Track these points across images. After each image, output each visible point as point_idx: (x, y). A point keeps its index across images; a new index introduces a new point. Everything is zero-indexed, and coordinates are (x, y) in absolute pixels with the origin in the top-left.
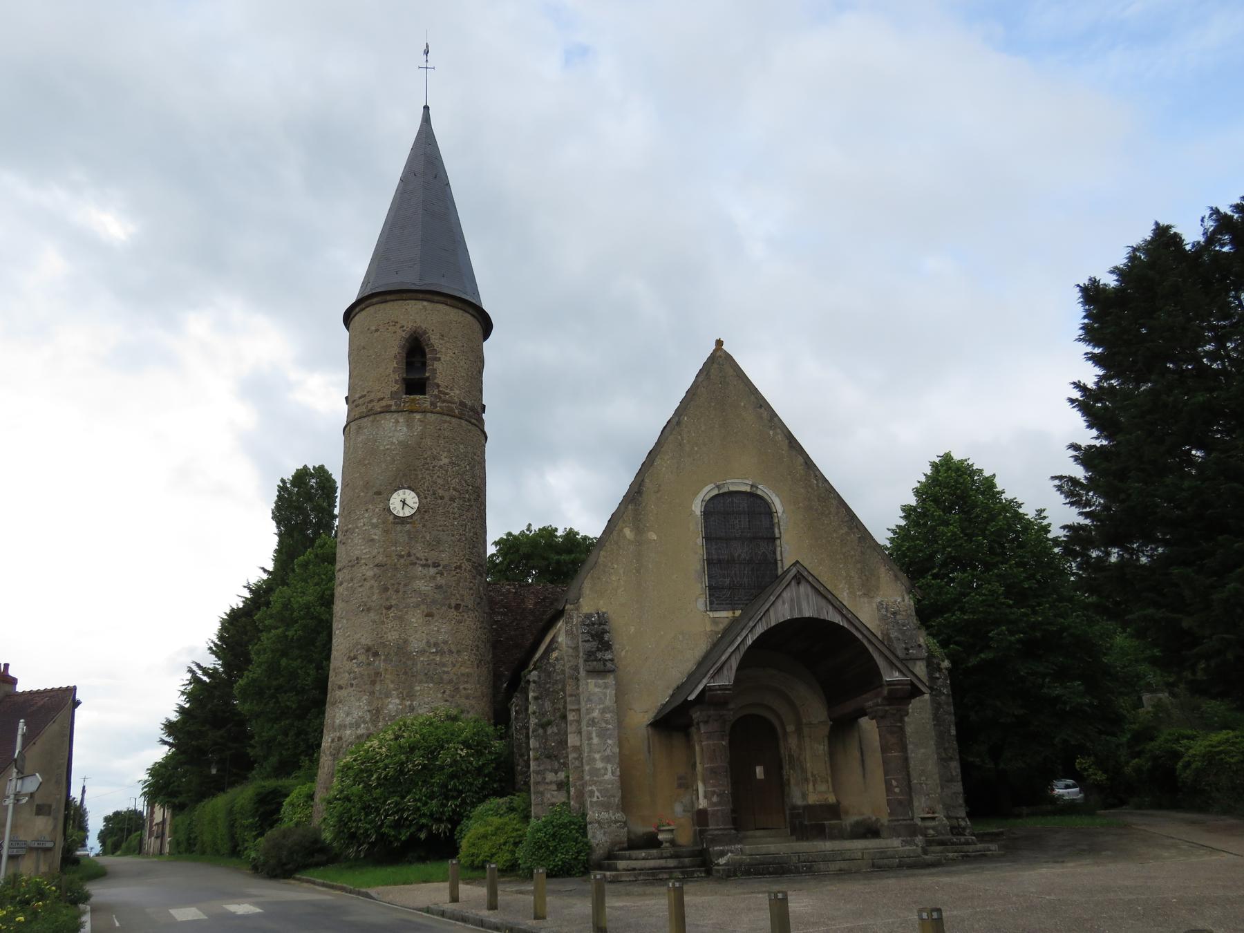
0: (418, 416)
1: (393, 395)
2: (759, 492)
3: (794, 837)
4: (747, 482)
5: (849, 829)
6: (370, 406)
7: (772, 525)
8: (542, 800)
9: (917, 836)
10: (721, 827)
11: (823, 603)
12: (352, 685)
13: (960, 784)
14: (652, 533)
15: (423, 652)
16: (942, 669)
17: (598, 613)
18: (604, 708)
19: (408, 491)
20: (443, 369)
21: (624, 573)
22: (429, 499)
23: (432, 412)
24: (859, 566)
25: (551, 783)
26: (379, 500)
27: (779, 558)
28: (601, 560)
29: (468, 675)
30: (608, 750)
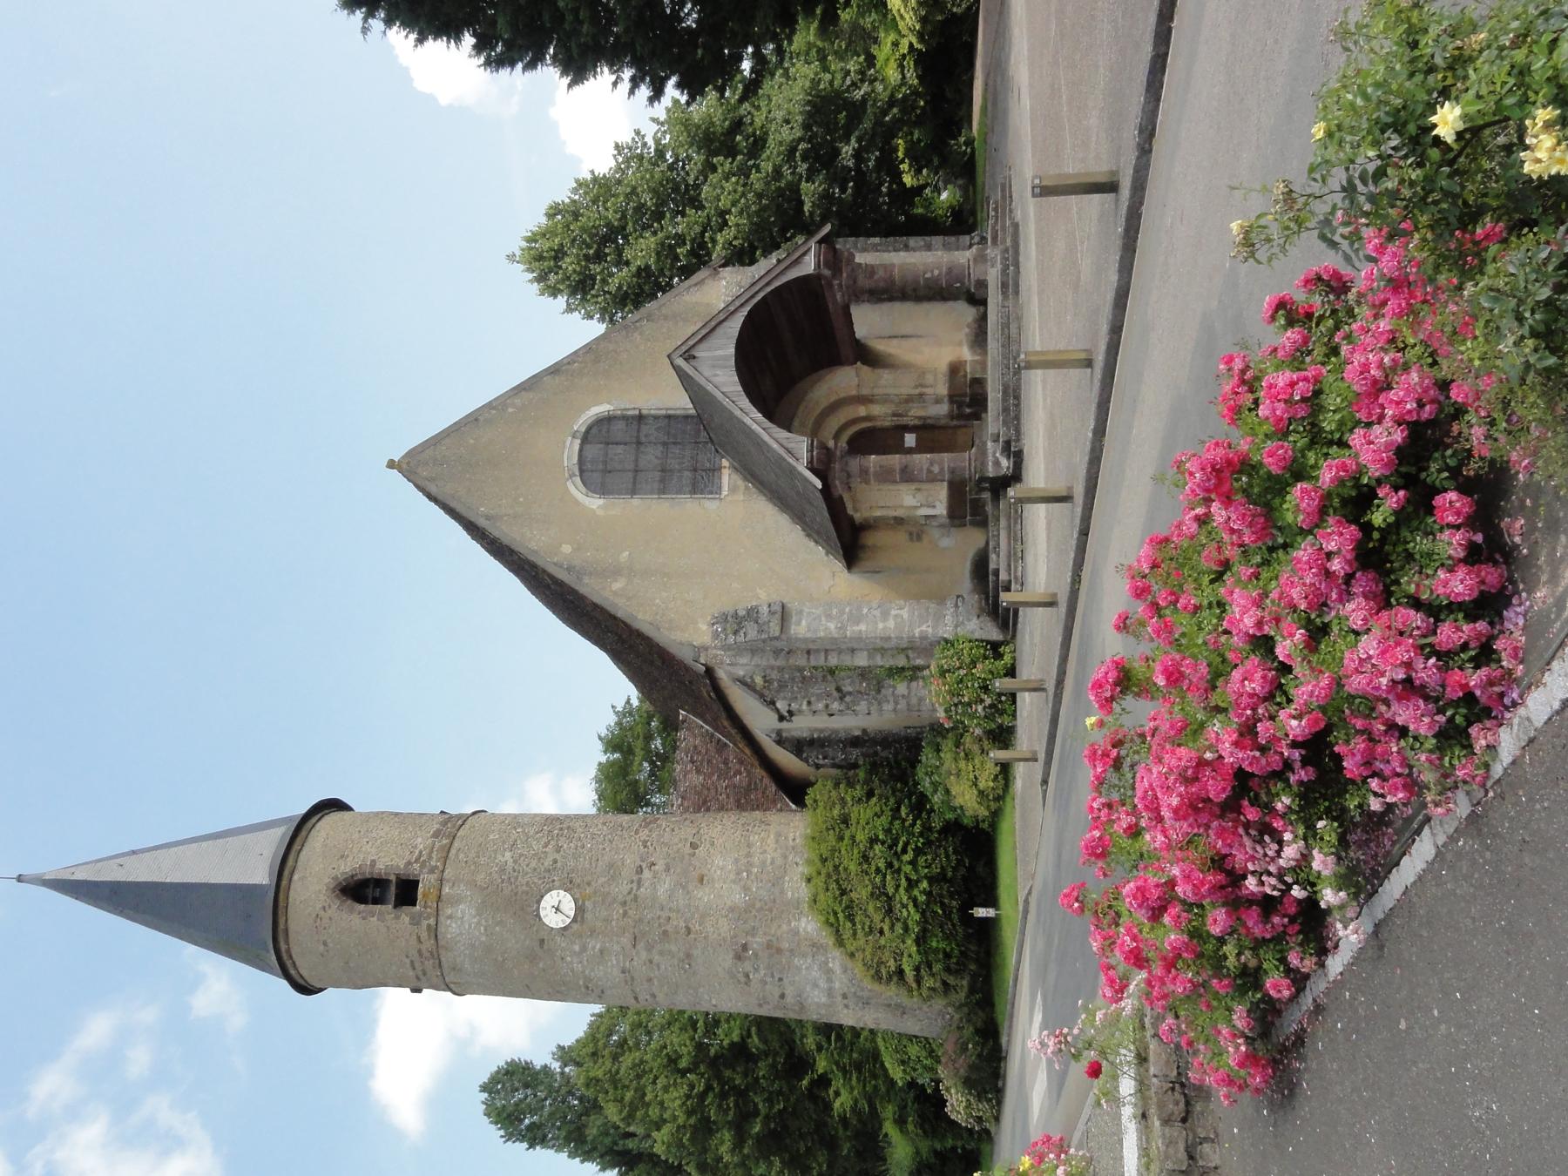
0: (446, 890)
2: (583, 430)
3: (983, 415)
4: (568, 443)
6: (426, 954)
7: (625, 418)
11: (720, 331)
12: (780, 979)
15: (746, 889)
19: (543, 904)
20: (388, 860)
27: (664, 412)
28: (648, 618)
29: (778, 835)
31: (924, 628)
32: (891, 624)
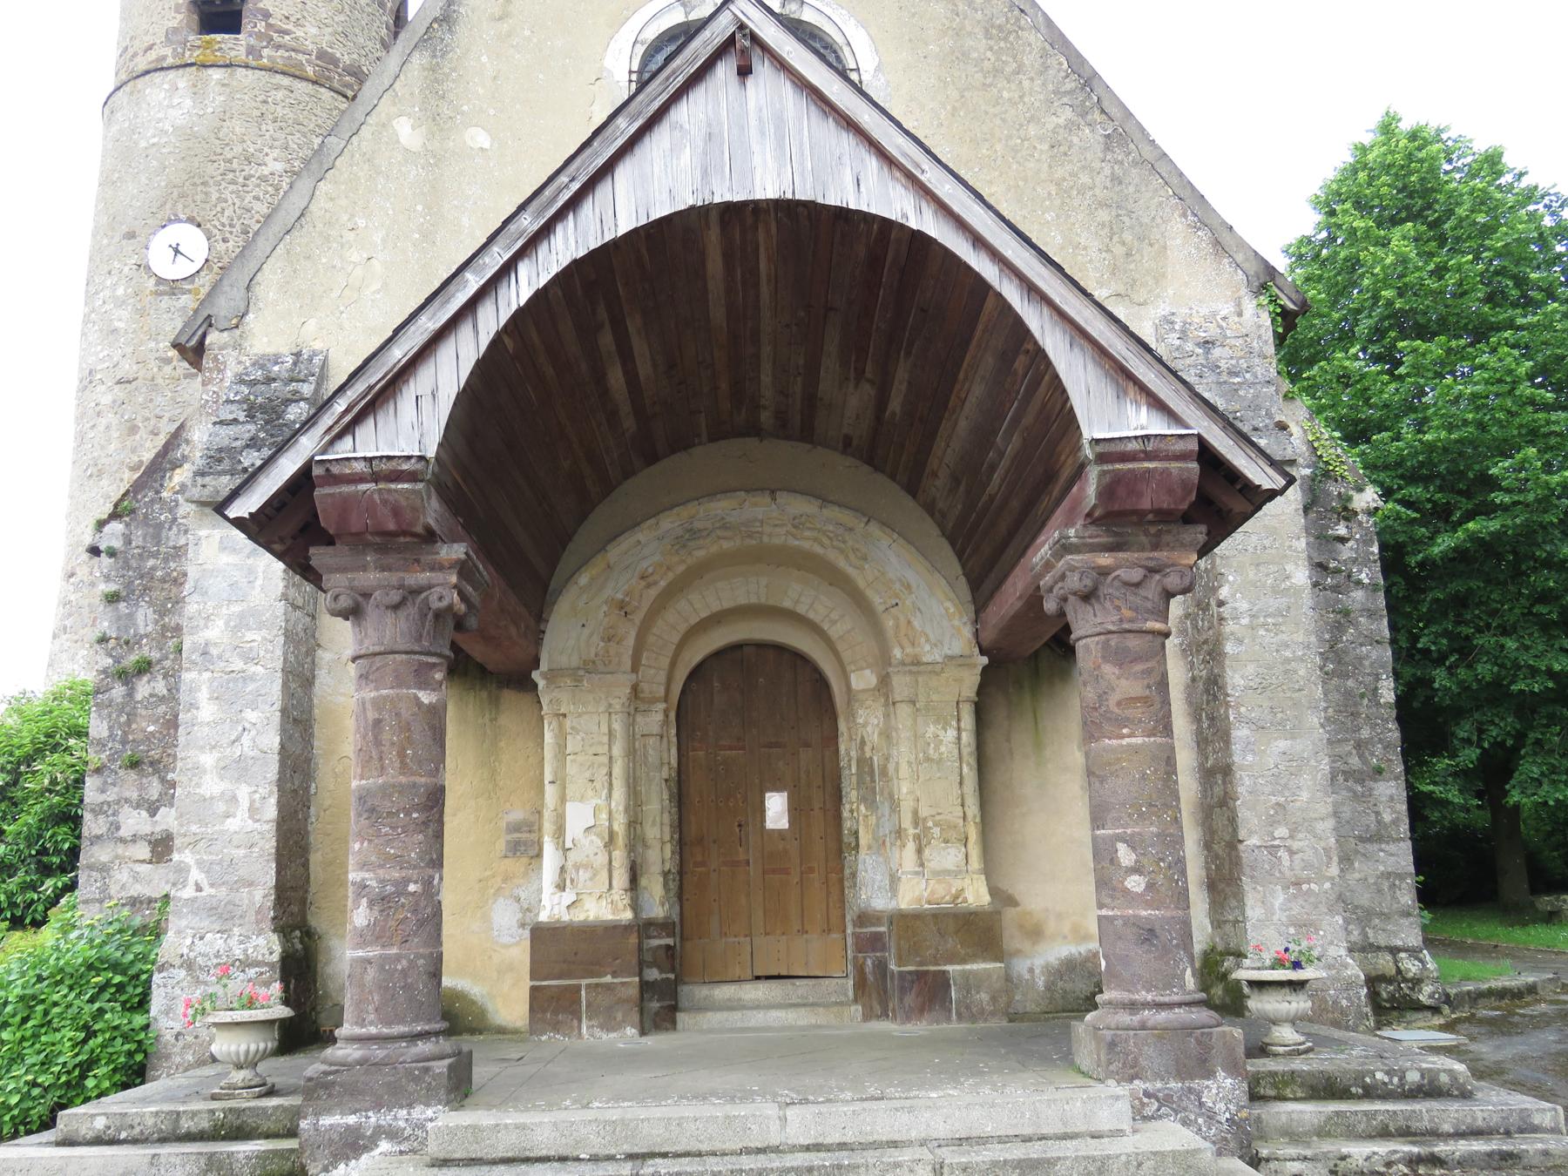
0: (216, 74)
1: (169, 36)
5: (1041, 983)
8: (104, 889)
9: (1210, 1074)
10: (373, 1030)
13: (1406, 847)
14: (473, 130)
16: (1356, 513)
17: (298, 355)
18: (242, 616)
21: (384, 241)
22: (231, 244)
23: (247, 67)
24: (1104, 215)
25: (135, 839)
26: (131, 248)
30: (246, 740)
31: (196, 875)
32: (212, 785)
